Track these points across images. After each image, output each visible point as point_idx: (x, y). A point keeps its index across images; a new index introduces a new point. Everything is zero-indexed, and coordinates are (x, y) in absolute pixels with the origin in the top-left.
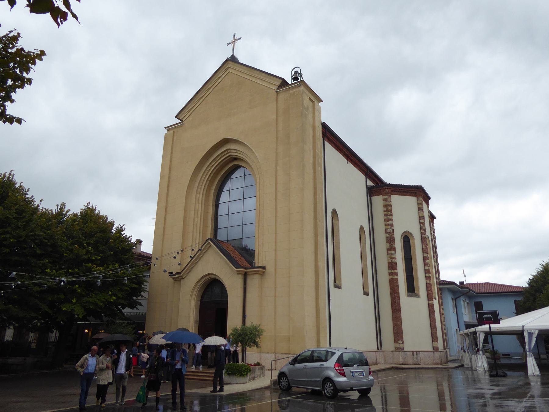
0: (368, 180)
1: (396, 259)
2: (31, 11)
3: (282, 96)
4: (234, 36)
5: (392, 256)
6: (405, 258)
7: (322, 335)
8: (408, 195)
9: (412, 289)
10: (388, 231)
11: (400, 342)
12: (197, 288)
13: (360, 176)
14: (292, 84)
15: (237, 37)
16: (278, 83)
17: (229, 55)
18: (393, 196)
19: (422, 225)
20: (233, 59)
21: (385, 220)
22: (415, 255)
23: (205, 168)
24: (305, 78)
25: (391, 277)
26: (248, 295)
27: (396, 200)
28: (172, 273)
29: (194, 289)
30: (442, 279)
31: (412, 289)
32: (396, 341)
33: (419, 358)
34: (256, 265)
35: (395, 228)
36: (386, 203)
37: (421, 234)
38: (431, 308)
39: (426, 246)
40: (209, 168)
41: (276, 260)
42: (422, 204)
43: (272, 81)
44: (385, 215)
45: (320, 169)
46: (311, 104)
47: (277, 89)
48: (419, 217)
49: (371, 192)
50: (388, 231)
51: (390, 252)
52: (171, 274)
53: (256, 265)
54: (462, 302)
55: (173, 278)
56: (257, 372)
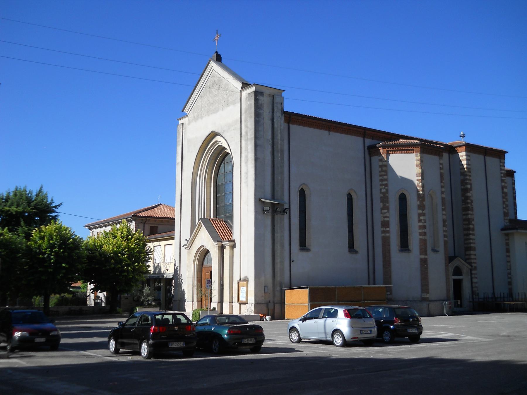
9: (405, 246)
25: (383, 235)
31: (405, 246)
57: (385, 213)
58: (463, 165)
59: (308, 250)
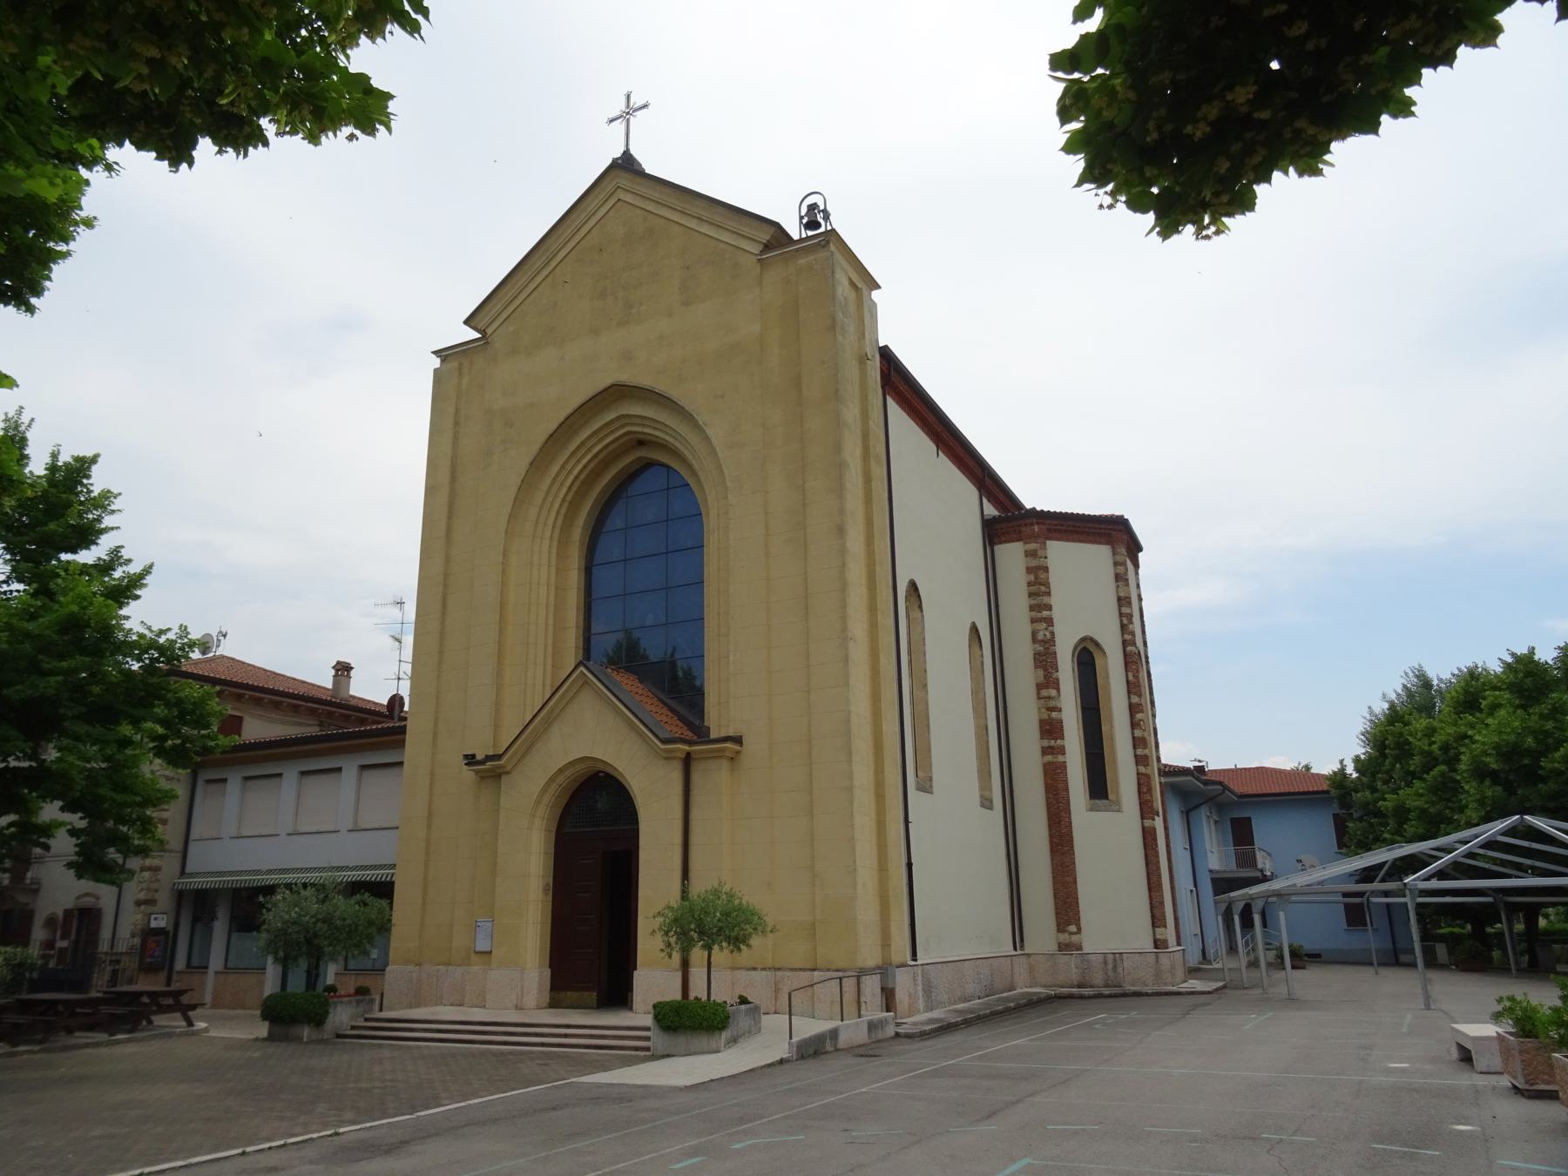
0: (985, 501)
1: (1060, 710)
2: (1168, 227)
4: (628, 97)
5: (1052, 704)
6: (1083, 709)
8: (1074, 541)
9: (1099, 787)
10: (1040, 636)
11: (1073, 928)
12: (546, 799)
13: (966, 490)
14: (801, 240)
15: (637, 101)
16: (765, 236)
18: (1049, 543)
20: (625, 165)
21: (1032, 608)
23: (555, 468)
24: (839, 223)
25: (1049, 758)
26: (695, 814)
27: (1061, 555)
28: (473, 756)
29: (538, 802)
31: (1099, 787)
32: (1061, 927)
33: (1120, 970)
34: (713, 735)
35: (1057, 629)
36: (1034, 563)
38: (1148, 837)
39: (1136, 677)
40: (569, 467)
42: (1124, 564)
43: (746, 231)
44: (1031, 595)
45: (879, 472)
46: (852, 295)
47: (762, 252)
48: (1119, 599)
50: (1040, 636)
51: (1044, 693)
52: (470, 760)
53: (713, 735)
54: (1204, 819)
55: (477, 772)
56: (742, 1021)
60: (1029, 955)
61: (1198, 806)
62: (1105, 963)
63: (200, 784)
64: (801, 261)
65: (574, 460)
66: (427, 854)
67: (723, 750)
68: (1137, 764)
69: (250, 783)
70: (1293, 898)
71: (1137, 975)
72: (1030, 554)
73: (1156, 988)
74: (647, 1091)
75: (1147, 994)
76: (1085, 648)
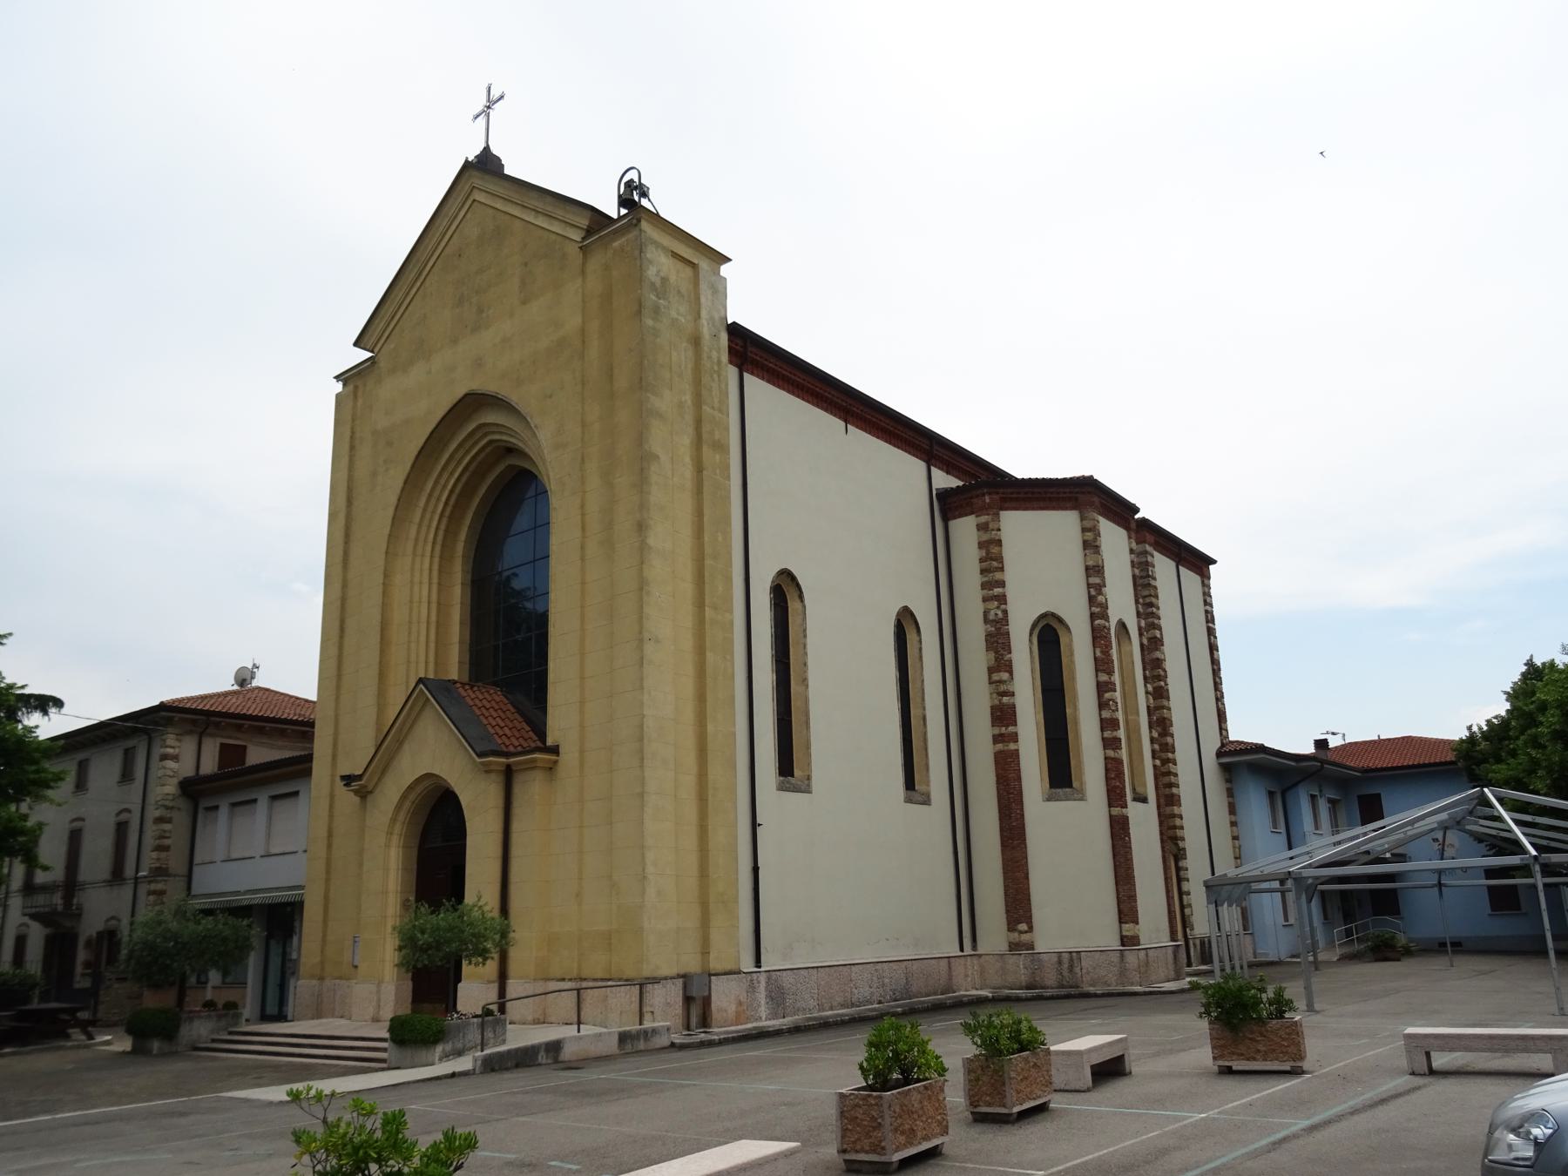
1: (1013, 694)
3: (596, 262)
5: (1003, 688)
7: (718, 921)
8: (1054, 508)
9: (1061, 775)
10: (992, 617)
11: (1023, 927)
12: (401, 817)
14: (620, 218)
15: (495, 94)
17: (472, 153)
19: (1093, 592)
20: (485, 165)
21: (984, 586)
22: (1073, 679)
25: (1000, 746)
26: (516, 826)
27: (1016, 525)
29: (394, 820)
30: (1232, 738)
31: (1061, 775)
32: (1011, 927)
33: (1077, 970)
35: (1011, 607)
36: (986, 537)
37: (1093, 616)
38: (1119, 829)
40: (442, 481)
41: (582, 727)
44: (983, 571)
47: (584, 239)
48: (1087, 568)
49: (947, 506)
50: (992, 617)
51: (995, 677)
57: (1000, 682)
58: (18, 801)
59: (805, 788)
60: (980, 956)
61: (1296, 785)
62: (1060, 962)
63: (200, 816)
64: (616, 244)
65: (445, 476)
66: (328, 872)
67: (534, 760)
68: (1105, 748)
69: (238, 809)
70: (1255, 886)
71: (1092, 975)
72: (982, 528)
73: (1120, 988)
74: (246, 1101)
75: (1096, 996)
76: (1048, 625)
